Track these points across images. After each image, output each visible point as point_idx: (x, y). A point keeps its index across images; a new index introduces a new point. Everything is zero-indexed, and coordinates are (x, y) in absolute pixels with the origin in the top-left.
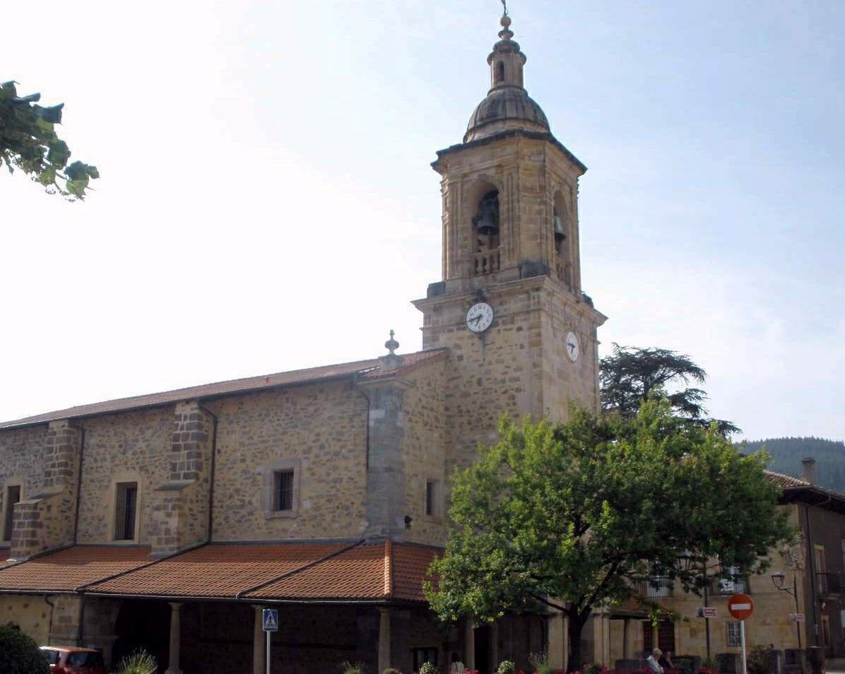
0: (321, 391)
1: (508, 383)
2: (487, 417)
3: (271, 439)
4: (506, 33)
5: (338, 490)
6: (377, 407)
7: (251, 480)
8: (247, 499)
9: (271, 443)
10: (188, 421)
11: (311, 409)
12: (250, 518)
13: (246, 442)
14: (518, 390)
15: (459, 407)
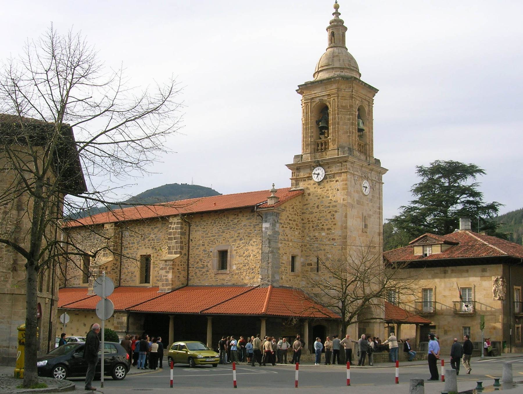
0: (241, 212)
1: (331, 208)
2: (321, 224)
3: (217, 235)
4: (337, 14)
5: (248, 261)
6: (266, 222)
7: (207, 255)
8: (205, 264)
9: (217, 237)
10: (175, 226)
11: (236, 221)
12: (207, 273)
13: (205, 236)
14: (336, 212)
15: (308, 219)
